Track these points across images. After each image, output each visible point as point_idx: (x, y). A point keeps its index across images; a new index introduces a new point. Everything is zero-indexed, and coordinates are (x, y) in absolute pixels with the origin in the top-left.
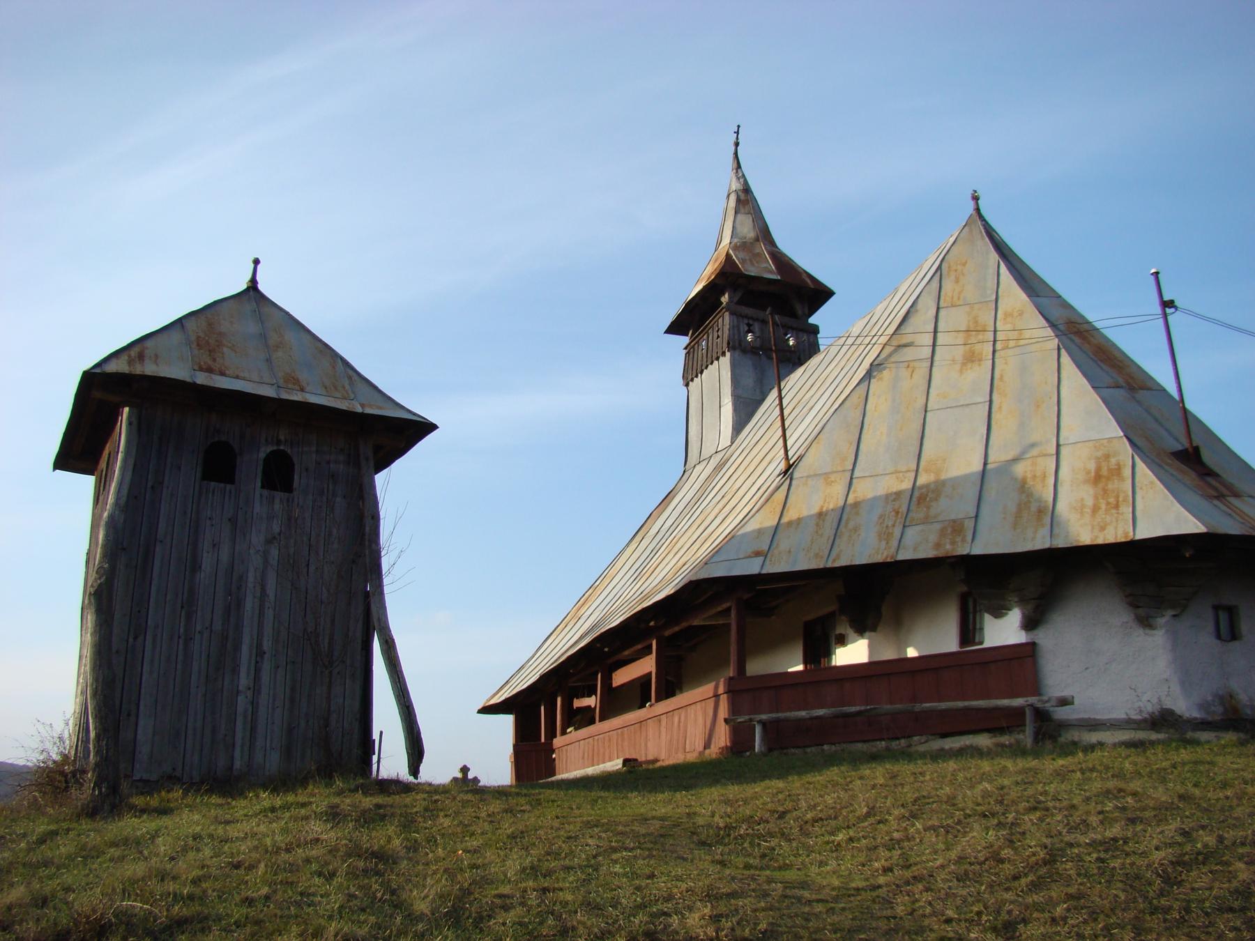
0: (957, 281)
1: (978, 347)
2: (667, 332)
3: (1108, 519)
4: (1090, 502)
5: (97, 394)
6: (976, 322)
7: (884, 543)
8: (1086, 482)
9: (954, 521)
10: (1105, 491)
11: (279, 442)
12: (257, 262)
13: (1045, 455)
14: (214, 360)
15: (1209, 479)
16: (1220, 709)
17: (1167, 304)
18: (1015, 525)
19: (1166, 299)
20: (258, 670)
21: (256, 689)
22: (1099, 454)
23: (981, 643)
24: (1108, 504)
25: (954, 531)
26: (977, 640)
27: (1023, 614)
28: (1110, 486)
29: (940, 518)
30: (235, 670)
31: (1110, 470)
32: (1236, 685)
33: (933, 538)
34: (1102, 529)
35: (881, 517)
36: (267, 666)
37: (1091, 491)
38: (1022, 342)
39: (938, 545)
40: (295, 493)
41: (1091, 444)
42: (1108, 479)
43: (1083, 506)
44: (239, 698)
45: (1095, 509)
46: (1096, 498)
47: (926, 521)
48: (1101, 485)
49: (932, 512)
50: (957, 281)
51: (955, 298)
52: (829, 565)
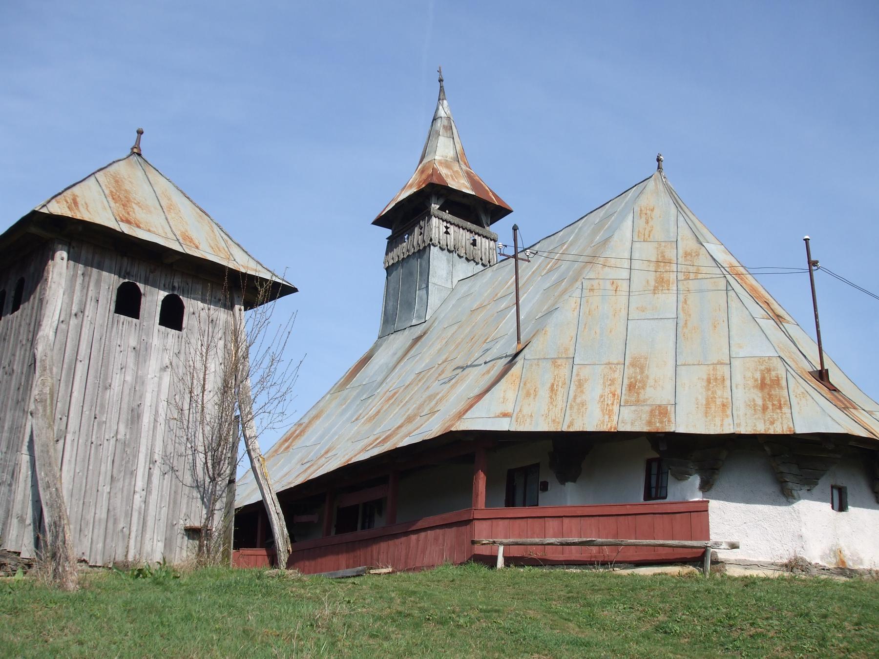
0: (647, 222)
1: (665, 275)
2: (373, 223)
3: (775, 416)
4: (760, 402)
5: (33, 230)
6: (663, 256)
7: (607, 417)
8: (755, 387)
9: (660, 406)
10: (770, 395)
11: (173, 288)
12: (140, 132)
13: (722, 364)
14: (128, 213)
15: (835, 393)
16: (834, 560)
17: (812, 264)
18: (706, 414)
19: (813, 259)
20: (150, 475)
21: (148, 489)
22: (763, 367)
23: (665, 498)
24: (773, 405)
25: (660, 413)
26: (663, 495)
27: (701, 479)
28: (773, 392)
29: (648, 402)
30: (133, 474)
31: (771, 380)
32: (843, 544)
33: (645, 417)
34: (772, 423)
35: (601, 396)
36: (156, 472)
37: (760, 395)
38: (700, 276)
39: (649, 423)
40: (184, 331)
41: (756, 359)
42: (771, 387)
43: (755, 405)
44: (136, 497)
45: (765, 408)
46: (764, 400)
47: (637, 402)
48: (766, 390)
49: (642, 397)
50: (647, 222)
51: (647, 236)
52: (565, 429)
